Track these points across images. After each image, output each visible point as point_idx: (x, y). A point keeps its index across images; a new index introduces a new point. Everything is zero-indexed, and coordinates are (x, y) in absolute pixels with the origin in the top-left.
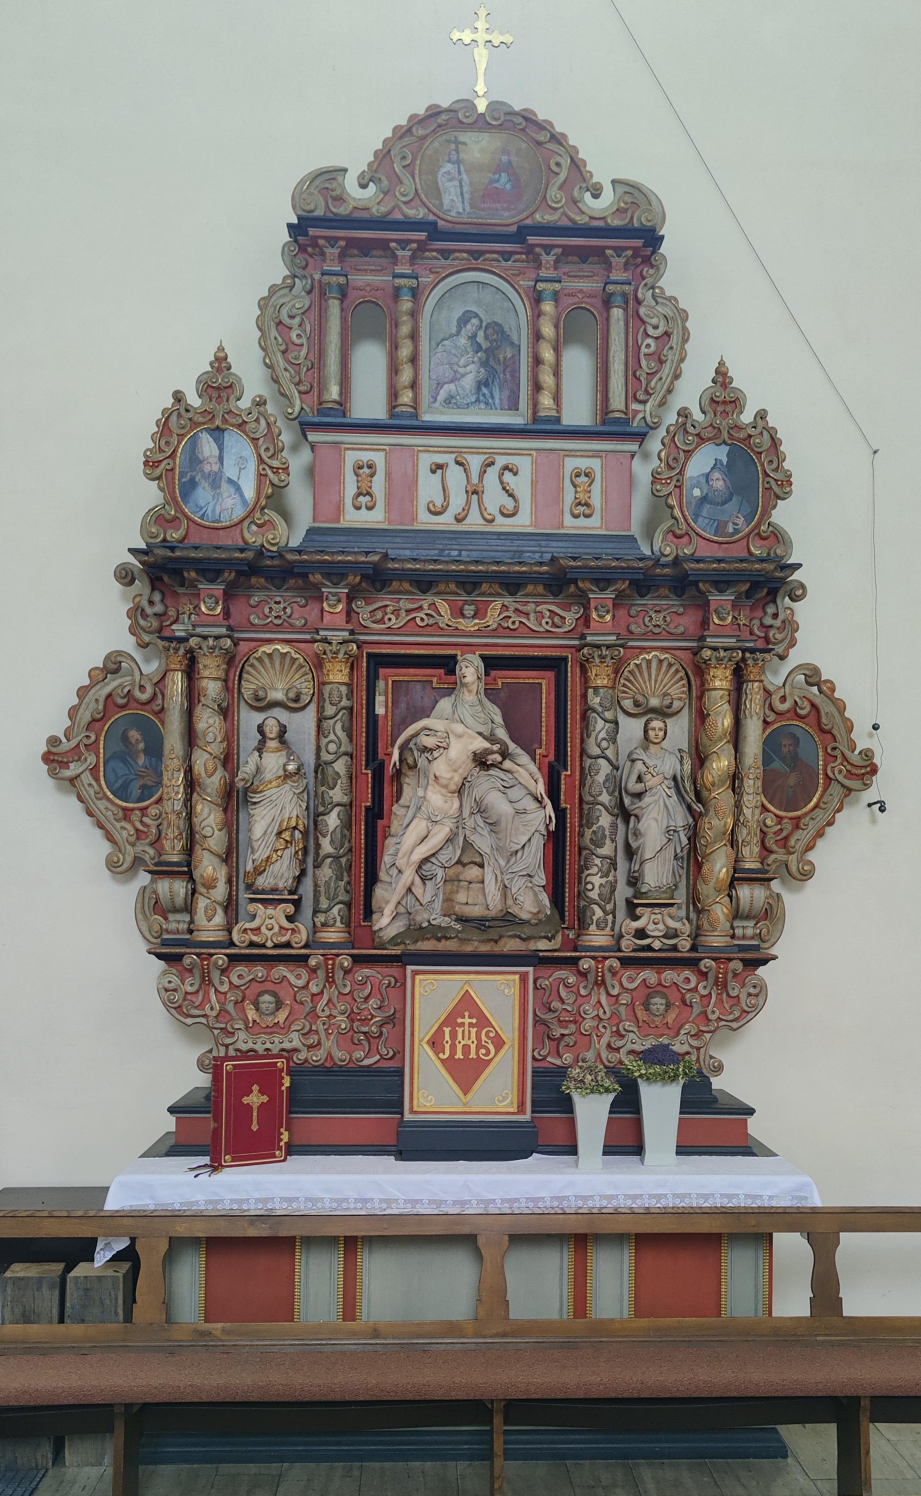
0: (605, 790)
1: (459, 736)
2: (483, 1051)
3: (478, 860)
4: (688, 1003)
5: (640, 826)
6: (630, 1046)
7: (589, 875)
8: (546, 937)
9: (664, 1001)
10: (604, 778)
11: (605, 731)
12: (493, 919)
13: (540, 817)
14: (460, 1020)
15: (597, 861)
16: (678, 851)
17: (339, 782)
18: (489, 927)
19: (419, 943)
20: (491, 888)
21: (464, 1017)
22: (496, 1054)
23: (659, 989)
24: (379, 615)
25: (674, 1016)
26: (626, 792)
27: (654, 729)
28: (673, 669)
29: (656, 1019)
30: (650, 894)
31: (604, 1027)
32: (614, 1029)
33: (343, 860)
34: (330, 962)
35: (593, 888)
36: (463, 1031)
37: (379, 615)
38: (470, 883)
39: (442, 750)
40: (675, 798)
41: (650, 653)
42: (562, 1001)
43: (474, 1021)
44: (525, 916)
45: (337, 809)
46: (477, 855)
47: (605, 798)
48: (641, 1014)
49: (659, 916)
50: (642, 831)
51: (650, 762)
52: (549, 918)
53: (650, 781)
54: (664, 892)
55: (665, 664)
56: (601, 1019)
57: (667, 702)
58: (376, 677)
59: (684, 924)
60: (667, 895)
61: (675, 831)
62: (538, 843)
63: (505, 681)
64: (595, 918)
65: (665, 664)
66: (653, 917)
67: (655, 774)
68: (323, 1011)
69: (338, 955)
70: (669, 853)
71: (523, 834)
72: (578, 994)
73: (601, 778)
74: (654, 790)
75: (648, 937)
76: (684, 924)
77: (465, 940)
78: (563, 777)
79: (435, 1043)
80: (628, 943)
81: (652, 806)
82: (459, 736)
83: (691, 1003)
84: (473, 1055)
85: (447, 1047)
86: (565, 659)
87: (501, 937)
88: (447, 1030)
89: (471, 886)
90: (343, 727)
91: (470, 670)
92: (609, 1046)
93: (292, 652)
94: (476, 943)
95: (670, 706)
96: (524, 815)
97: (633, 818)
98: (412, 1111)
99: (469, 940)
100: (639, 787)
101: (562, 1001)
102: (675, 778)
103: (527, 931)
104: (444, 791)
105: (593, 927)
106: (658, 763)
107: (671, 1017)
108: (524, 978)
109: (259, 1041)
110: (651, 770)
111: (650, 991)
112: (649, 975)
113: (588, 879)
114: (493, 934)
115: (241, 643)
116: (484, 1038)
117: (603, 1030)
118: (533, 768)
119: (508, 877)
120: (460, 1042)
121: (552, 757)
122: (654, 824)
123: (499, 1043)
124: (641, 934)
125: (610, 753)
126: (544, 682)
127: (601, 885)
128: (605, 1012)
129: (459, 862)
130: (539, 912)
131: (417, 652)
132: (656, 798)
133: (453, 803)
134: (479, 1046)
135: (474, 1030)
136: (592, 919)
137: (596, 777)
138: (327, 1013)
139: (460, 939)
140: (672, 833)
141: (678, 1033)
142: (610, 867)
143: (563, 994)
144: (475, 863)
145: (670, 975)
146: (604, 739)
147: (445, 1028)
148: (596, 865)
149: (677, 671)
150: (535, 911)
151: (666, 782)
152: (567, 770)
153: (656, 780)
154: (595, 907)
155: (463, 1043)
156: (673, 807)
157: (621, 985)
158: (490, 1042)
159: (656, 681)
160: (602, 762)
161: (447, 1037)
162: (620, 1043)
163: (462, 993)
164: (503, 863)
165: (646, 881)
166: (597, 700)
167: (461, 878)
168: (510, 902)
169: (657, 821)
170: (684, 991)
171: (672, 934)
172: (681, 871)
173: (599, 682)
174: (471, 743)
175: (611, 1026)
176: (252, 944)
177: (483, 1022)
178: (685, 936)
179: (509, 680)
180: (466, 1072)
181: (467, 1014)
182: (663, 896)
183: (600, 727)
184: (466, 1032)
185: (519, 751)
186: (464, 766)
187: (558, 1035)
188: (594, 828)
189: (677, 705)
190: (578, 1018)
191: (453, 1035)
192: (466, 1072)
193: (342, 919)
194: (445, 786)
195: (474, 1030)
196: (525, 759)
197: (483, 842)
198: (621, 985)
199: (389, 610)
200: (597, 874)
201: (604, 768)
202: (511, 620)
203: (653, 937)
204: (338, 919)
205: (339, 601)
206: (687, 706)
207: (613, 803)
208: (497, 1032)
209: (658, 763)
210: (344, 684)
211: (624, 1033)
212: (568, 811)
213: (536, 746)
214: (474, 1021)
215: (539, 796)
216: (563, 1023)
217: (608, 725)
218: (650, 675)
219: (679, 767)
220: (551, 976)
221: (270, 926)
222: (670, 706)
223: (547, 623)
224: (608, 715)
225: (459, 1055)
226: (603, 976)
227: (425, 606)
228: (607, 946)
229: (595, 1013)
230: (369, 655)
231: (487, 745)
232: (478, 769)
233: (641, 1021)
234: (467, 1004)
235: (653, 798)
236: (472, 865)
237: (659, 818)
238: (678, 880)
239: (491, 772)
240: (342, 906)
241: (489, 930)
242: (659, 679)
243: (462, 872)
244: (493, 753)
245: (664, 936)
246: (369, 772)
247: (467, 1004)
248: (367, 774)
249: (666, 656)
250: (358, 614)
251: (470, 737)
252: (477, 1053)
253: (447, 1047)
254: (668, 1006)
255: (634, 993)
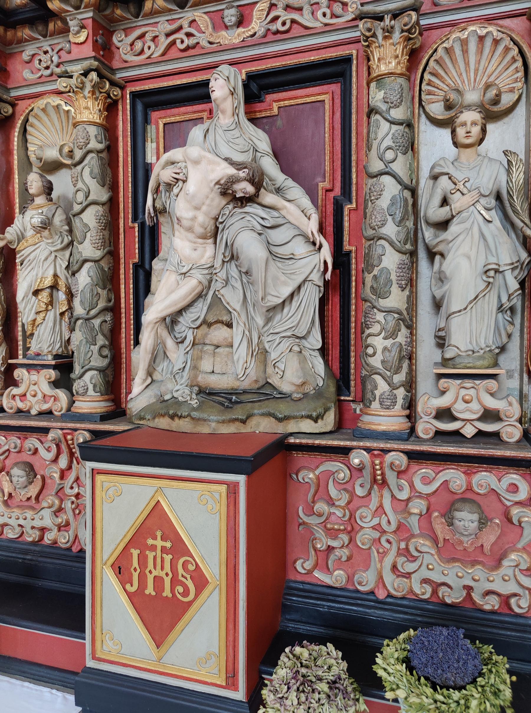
0: (390, 218)
1: (196, 162)
2: (180, 589)
3: (225, 318)
4: (515, 521)
5: (444, 267)
6: (425, 573)
7: (369, 335)
8: (309, 417)
9: (475, 517)
10: (388, 202)
11: (390, 136)
12: (245, 392)
13: (312, 263)
14: (150, 542)
15: (380, 316)
16: (504, 299)
17: (88, 235)
18: (237, 403)
19: (157, 420)
20: (242, 352)
21: (155, 538)
22: (197, 596)
23: (468, 498)
24: (139, 45)
25: (492, 538)
26: (428, 223)
27: (464, 124)
28: (500, 48)
29: (465, 539)
30: (457, 360)
31: (389, 541)
32: (403, 545)
33: (97, 322)
34: (69, 437)
35: (374, 354)
36: (155, 558)
37: (139, 45)
38: (218, 347)
39: (180, 183)
40: (497, 222)
41: (464, 29)
42: (331, 502)
43: (168, 544)
44: (286, 388)
45: (87, 265)
46: (224, 312)
47: (390, 229)
48: (440, 527)
49: (472, 392)
50: (448, 273)
51: (459, 175)
52: (319, 394)
53: (458, 202)
54: (482, 358)
55: (488, 42)
56: (384, 532)
57: (492, 93)
58: (146, 121)
59: (510, 404)
60: (486, 363)
61: (496, 271)
62: (311, 297)
63: (282, 104)
64: (377, 393)
65: (488, 42)
66: (463, 392)
67: (465, 191)
68: (72, 488)
69: (76, 430)
70: (490, 303)
71: (285, 284)
72: (352, 494)
73: (384, 202)
74: (464, 214)
75: (455, 419)
76: (510, 404)
77: (199, 419)
78: (346, 212)
79: (120, 569)
80: (426, 426)
81: (461, 238)
82: (196, 162)
83: (520, 522)
84: (167, 593)
85: (135, 576)
86: (347, 60)
87: (250, 416)
88: (135, 553)
89: (218, 350)
90: (91, 173)
91: (224, 86)
92: (394, 568)
93: (63, 103)
94: (213, 425)
95: (496, 101)
96: (293, 261)
97: (438, 257)
98: (94, 658)
99: (205, 420)
100: (443, 213)
101: (331, 502)
102: (498, 197)
103: (283, 409)
104: (190, 236)
105: (375, 405)
106: (472, 174)
107: (489, 538)
108: (233, 489)
109: (14, 515)
110: (461, 186)
111: (450, 503)
112: (455, 477)
113: (370, 340)
114: (239, 413)
115: (20, 102)
116: (181, 571)
117: (387, 545)
118: (306, 202)
119: (269, 338)
120: (150, 572)
121: (338, 191)
122: (464, 264)
123: (201, 582)
124: (445, 414)
125: (399, 167)
126: (326, 98)
127: (385, 349)
128: (389, 522)
129: (204, 322)
130: (304, 384)
131: (179, 82)
132: (467, 225)
133: (205, 251)
134: (175, 582)
135: (168, 558)
136: (373, 393)
137: (377, 202)
138: (76, 490)
139: (193, 419)
140: (492, 273)
141: (498, 564)
142: (398, 325)
143: (333, 492)
144: (222, 322)
145: (484, 479)
146: (389, 148)
147: (132, 550)
148: (378, 322)
149: (507, 49)
150: (299, 381)
151: (483, 201)
152: (351, 202)
153: (468, 199)
154: (377, 378)
155: (155, 573)
156: (494, 237)
157: (412, 486)
158: (188, 577)
159: (476, 70)
160: (387, 180)
161: (135, 564)
162: (410, 567)
163: (153, 504)
164: (260, 321)
165: (453, 342)
166: (381, 95)
167: (207, 342)
168: (270, 370)
169: (469, 258)
170: (508, 504)
171: (490, 415)
172: (510, 329)
173: (383, 69)
174: (213, 171)
175: (399, 541)
176: (19, 411)
177: (179, 548)
178: (513, 421)
179: (287, 103)
180: (161, 615)
181: (159, 534)
182: (479, 363)
183: (385, 134)
184: (159, 560)
185: (290, 183)
186: (208, 202)
187: (324, 547)
188: (376, 272)
189: (507, 100)
190: (352, 529)
191: (143, 560)
192: (161, 615)
193: (95, 386)
194: (190, 229)
195: (168, 558)
196: (296, 191)
197: (232, 298)
198: (412, 486)
199: (148, 37)
200: (379, 334)
201: (390, 188)
202: (280, 21)
203: (463, 420)
204: (91, 387)
205: (83, 27)
206: (524, 95)
207: (402, 236)
208: (197, 564)
209: (472, 174)
210: (94, 124)
211: (415, 554)
212: (353, 255)
213: (319, 179)
214: (168, 544)
215: (310, 236)
216: (332, 533)
217: (395, 128)
218: (467, 64)
219: (503, 178)
220: (317, 467)
221: (33, 393)
222: (496, 101)
223: (324, 15)
224: (397, 114)
225: (150, 590)
226: (383, 474)
227: (185, 25)
228: (393, 432)
229: (376, 521)
230: (135, 95)
231: (232, 171)
232: (230, 207)
233: (441, 540)
234: (155, 521)
235: (462, 226)
236: (219, 325)
237: (473, 254)
238: (505, 339)
239: (247, 209)
240: (96, 372)
241: (235, 407)
242: (481, 68)
243: (206, 335)
244: (238, 180)
245: (479, 419)
246: (136, 225)
247: (155, 521)
248: (134, 228)
249: (491, 29)
250: (119, 48)
251: (210, 162)
252: (172, 590)
253: (135, 576)
254: (483, 522)
255: (433, 500)
